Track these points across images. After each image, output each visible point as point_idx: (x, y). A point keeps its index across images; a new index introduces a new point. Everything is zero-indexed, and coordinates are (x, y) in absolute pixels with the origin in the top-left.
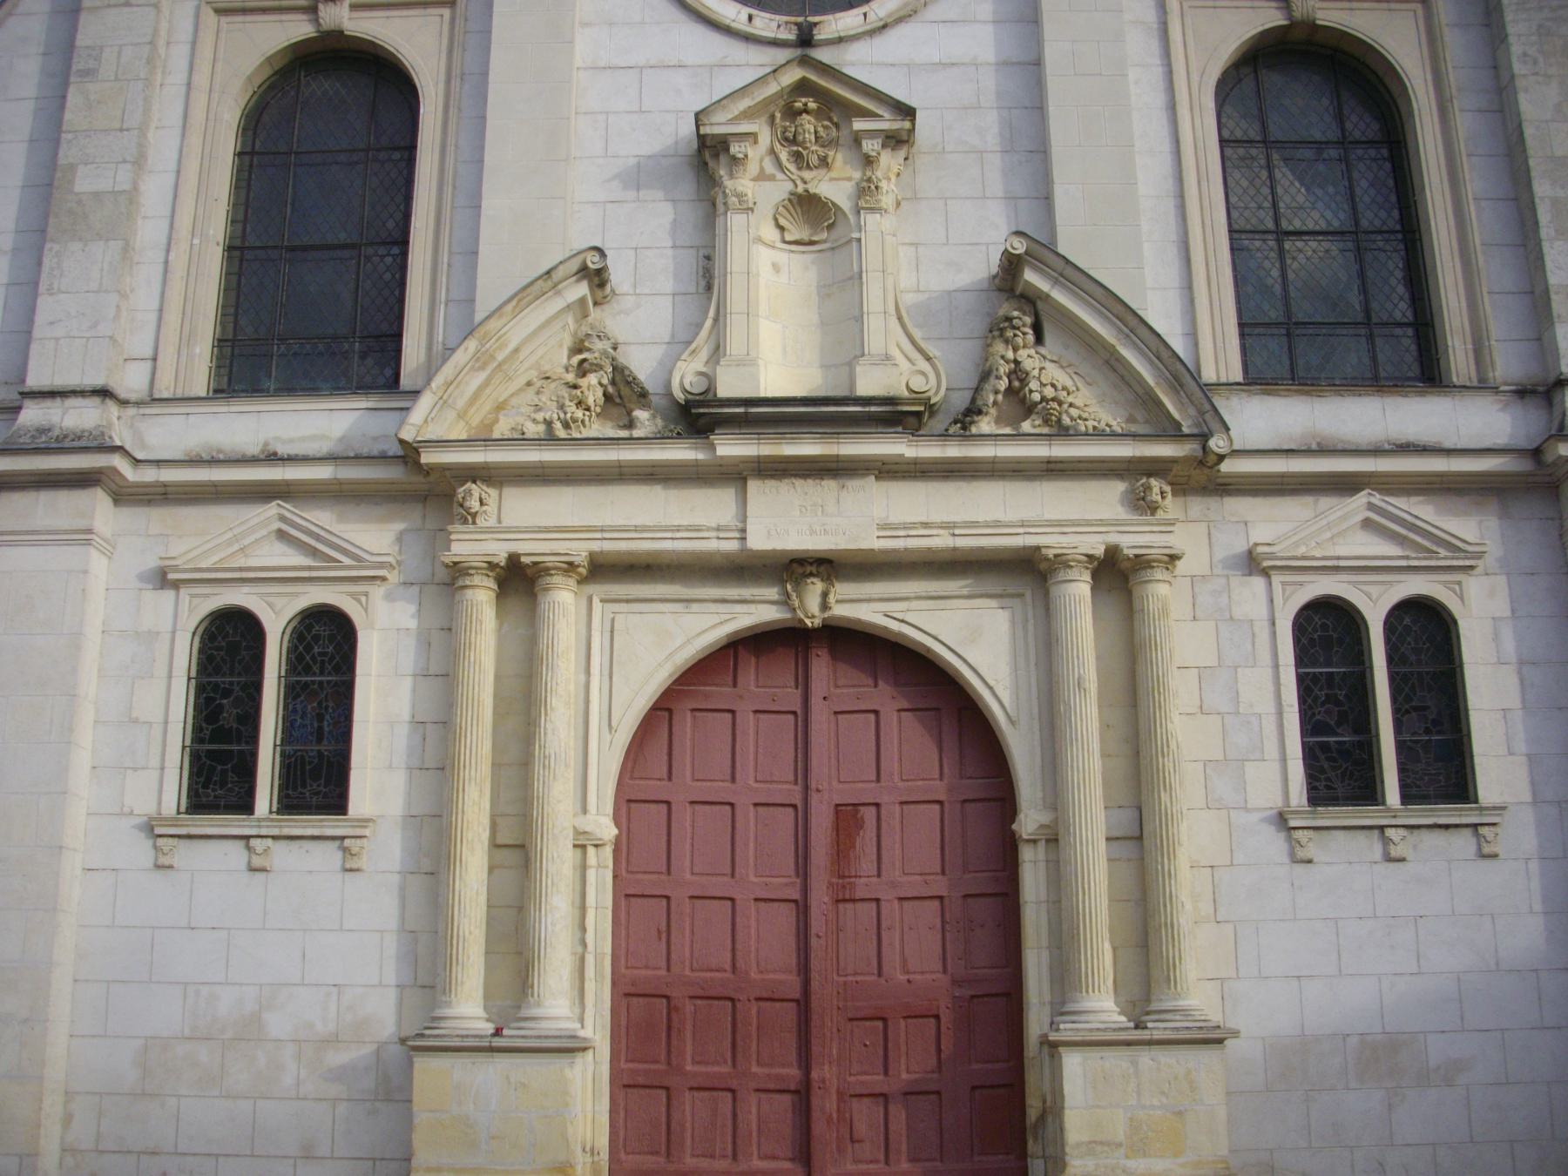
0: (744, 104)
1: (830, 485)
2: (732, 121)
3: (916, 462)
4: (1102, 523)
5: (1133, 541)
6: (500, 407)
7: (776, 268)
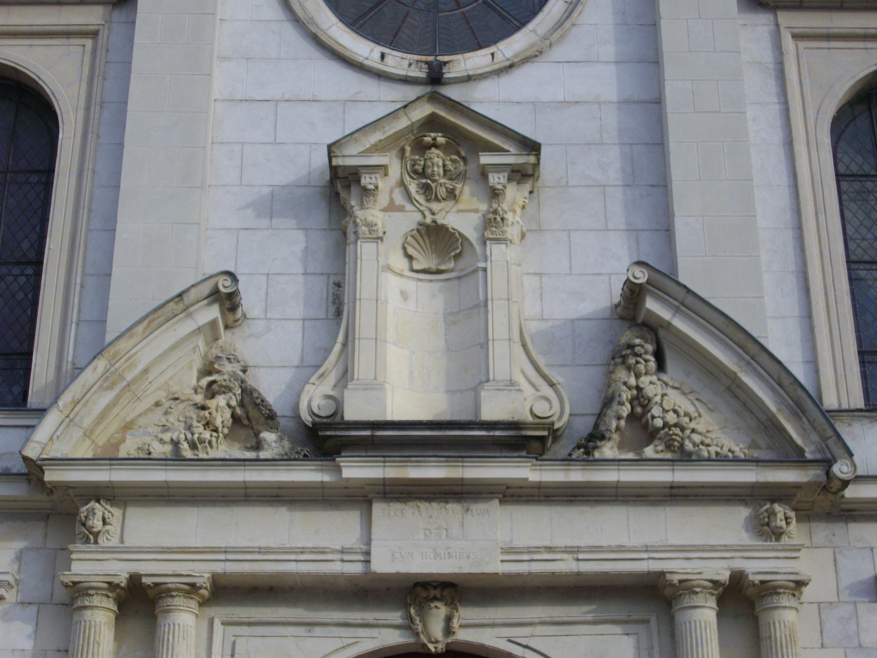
0: (376, 137)
1: (454, 509)
2: (362, 154)
3: (539, 486)
4: (726, 548)
5: (759, 565)
6: (127, 427)
7: (404, 295)
